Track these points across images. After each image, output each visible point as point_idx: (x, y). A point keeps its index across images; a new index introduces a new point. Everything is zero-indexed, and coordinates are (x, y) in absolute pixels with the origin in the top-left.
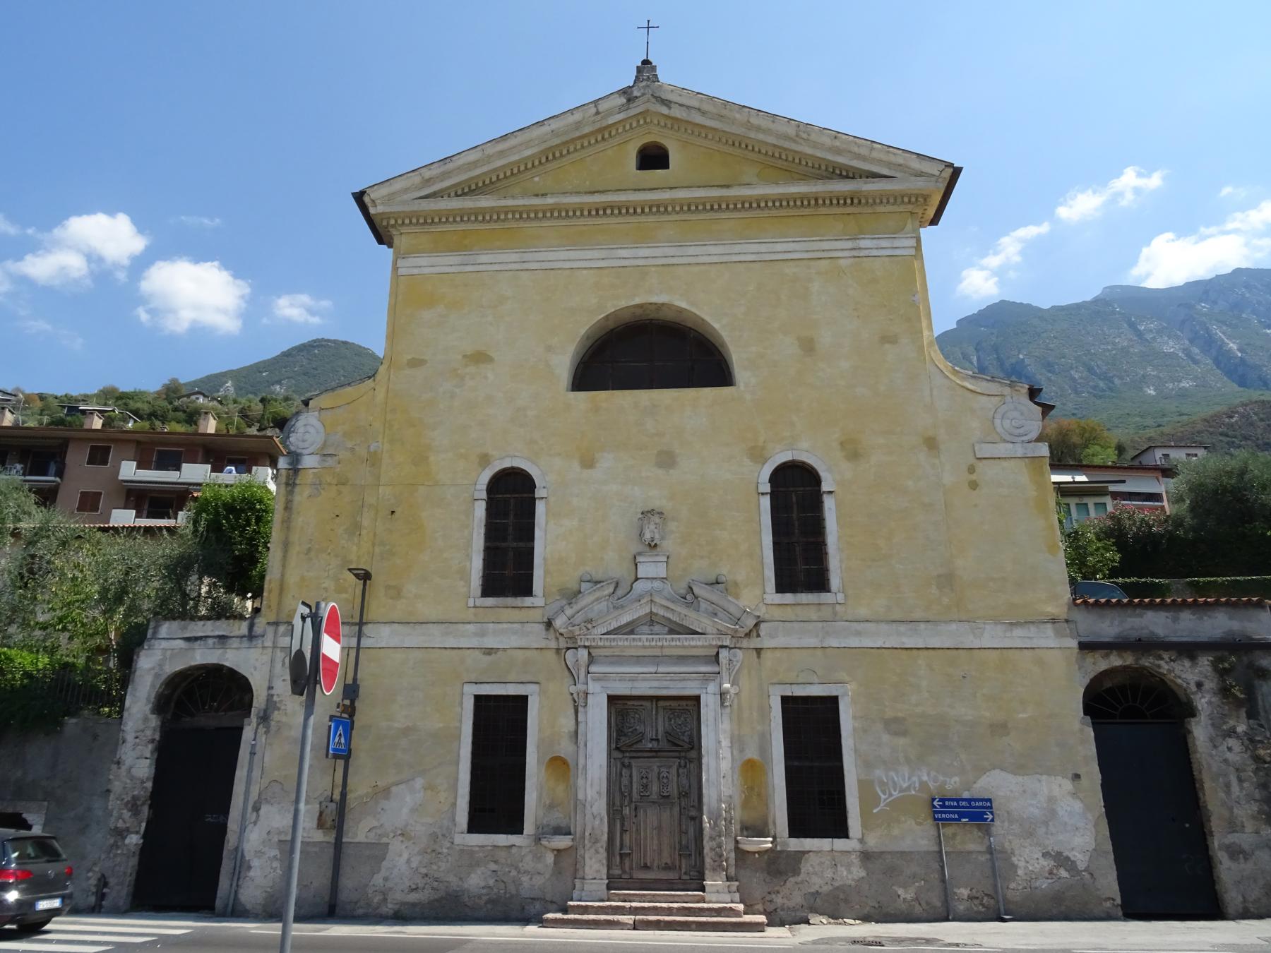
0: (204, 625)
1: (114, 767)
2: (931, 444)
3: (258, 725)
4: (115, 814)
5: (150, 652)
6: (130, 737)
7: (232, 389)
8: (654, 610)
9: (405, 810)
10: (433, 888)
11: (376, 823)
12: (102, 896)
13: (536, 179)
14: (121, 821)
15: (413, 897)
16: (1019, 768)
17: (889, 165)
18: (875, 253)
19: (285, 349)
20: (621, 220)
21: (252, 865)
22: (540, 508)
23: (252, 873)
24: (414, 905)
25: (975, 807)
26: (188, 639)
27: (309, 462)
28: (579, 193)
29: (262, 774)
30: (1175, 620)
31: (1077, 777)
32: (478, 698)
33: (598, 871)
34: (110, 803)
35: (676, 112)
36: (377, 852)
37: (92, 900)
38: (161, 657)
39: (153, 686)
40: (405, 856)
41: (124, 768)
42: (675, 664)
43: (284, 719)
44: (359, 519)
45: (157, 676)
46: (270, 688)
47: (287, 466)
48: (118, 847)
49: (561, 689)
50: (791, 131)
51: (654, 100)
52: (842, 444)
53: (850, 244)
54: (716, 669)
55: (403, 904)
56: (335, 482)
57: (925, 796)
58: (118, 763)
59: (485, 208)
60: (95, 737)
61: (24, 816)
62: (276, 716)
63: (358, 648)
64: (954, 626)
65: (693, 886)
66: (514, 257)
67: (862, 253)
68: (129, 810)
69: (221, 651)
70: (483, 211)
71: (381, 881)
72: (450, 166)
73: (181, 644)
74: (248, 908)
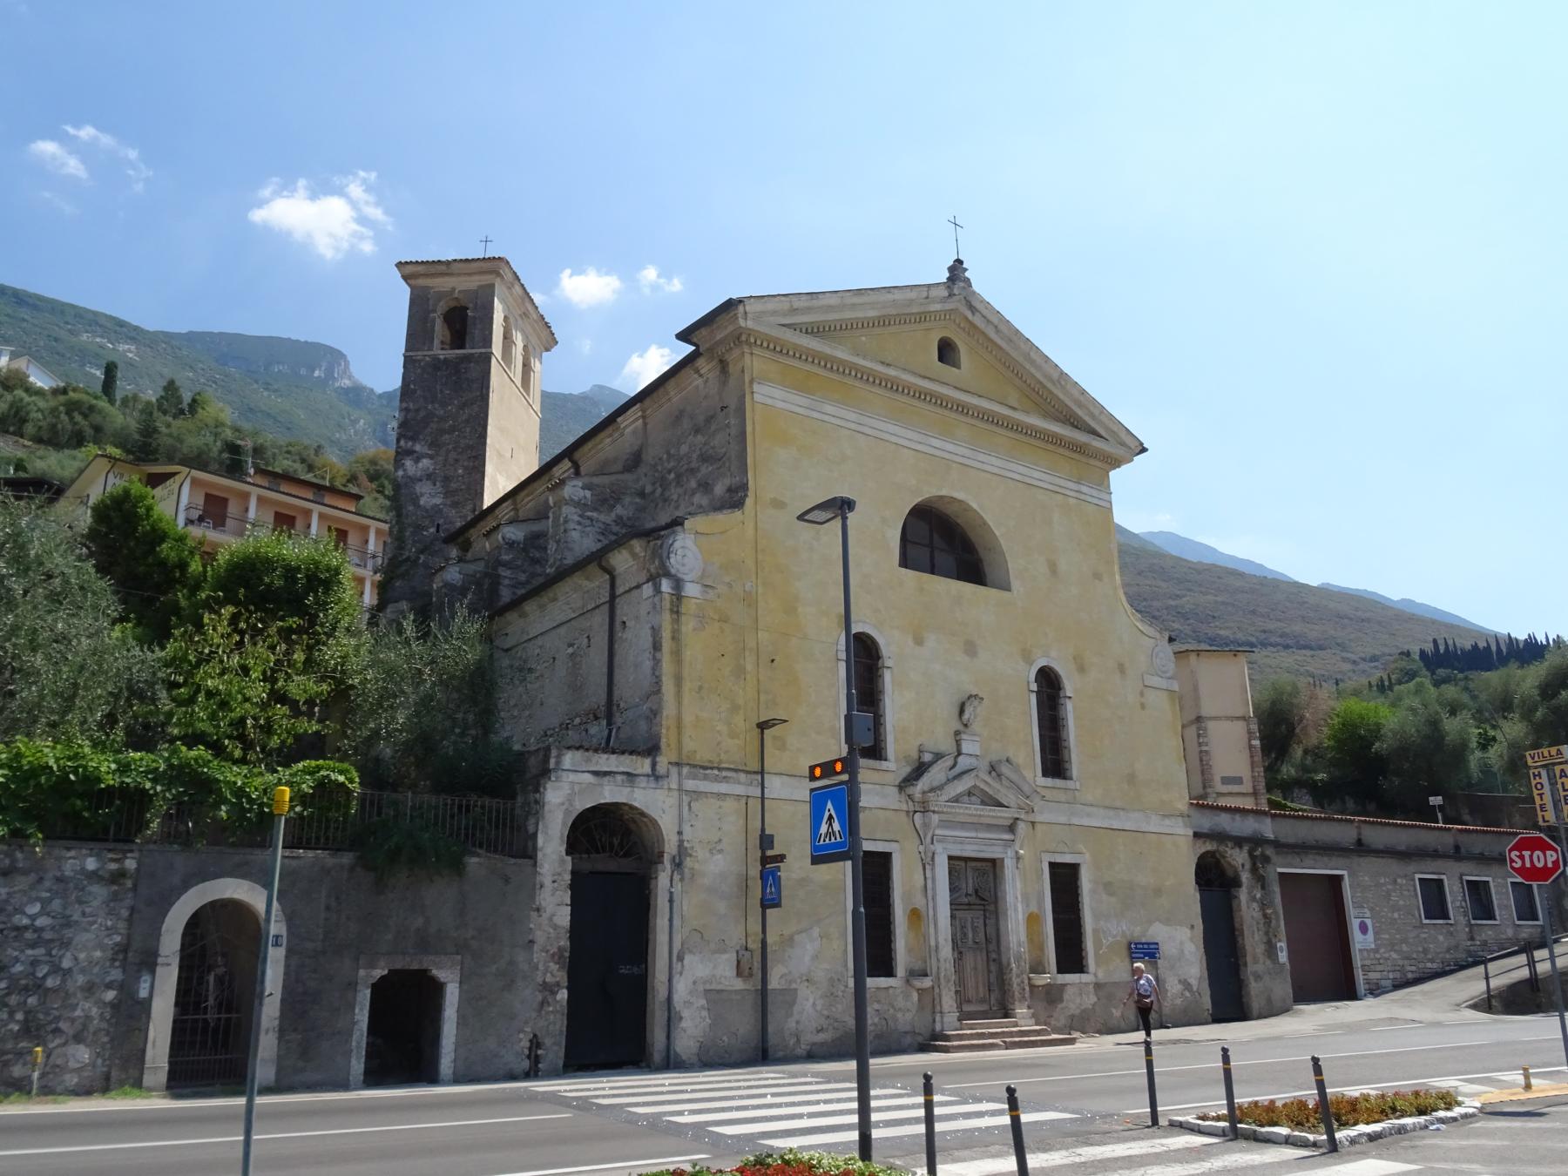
0: (607, 759)
1: (534, 914)
2: (1121, 668)
3: (673, 872)
4: (541, 967)
5: (556, 784)
6: (547, 881)
8: (978, 784)
9: (807, 959)
10: (834, 1028)
11: (785, 971)
12: (535, 1060)
13: (864, 338)
14: (549, 975)
15: (821, 1037)
16: (1167, 922)
17: (1107, 429)
18: (1090, 499)
20: (931, 408)
21: (683, 1015)
22: (887, 677)
23: (684, 1024)
24: (822, 1044)
26: (596, 773)
27: (691, 590)
28: (915, 374)
29: (683, 922)
30: (1233, 820)
31: (1192, 927)
33: (951, 1006)
34: (535, 955)
35: (977, 320)
36: (790, 996)
37: (526, 1064)
38: (569, 792)
39: (564, 824)
40: (811, 1001)
41: (545, 916)
43: (697, 866)
44: (742, 662)
45: (567, 812)
46: (680, 833)
47: (670, 591)
48: (549, 1004)
49: (912, 845)
50: (1055, 376)
51: (964, 302)
52: (1074, 658)
54: (1011, 837)
55: (814, 1044)
56: (716, 617)
57: (1125, 942)
58: (538, 910)
59: (836, 357)
60: (507, 880)
61: (435, 972)
62: (688, 862)
65: (1000, 1015)
66: (852, 416)
67: (1083, 497)
68: (556, 963)
69: (629, 789)
70: (833, 359)
71: (794, 1025)
72: (815, 303)
73: (588, 778)
74: (684, 1058)
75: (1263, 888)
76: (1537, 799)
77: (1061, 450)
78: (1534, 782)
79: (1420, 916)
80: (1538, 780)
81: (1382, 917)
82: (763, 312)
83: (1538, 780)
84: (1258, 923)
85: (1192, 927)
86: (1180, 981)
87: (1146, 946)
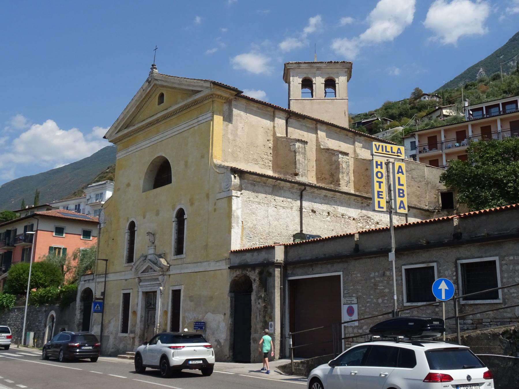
2: (208, 196)
7: (484, 73)
16: (214, 312)
19: (511, 37)
25: (201, 325)
31: (225, 314)
32: (124, 294)
42: (154, 281)
53: (196, 121)
63: (105, 282)
64: (205, 263)
66: (134, 148)
75: (265, 291)
76: (376, 185)
77: (192, 108)
78: (375, 170)
79: (403, 300)
80: (379, 169)
81: (368, 302)
82: (111, 134)
83: (379, 169)
84: (260, 311)
85: (225, 314)
86: (216, 341)
87: (199, 324)
